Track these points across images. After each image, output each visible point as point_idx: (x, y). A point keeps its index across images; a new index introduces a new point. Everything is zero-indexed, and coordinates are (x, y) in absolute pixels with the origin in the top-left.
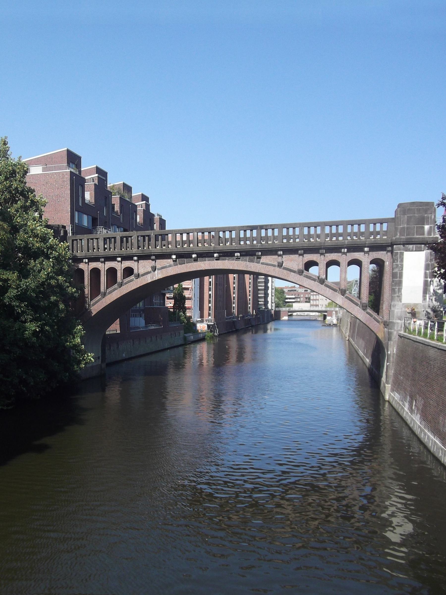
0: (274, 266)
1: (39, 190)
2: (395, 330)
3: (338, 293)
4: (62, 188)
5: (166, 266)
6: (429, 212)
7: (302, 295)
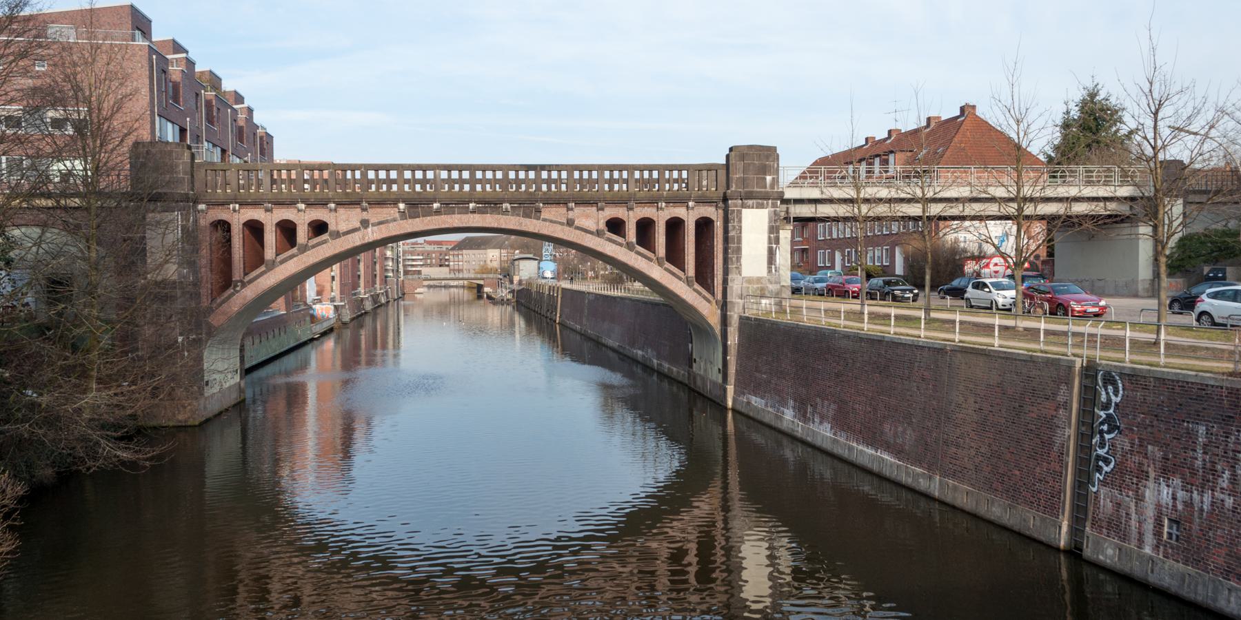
0: (562, 224)
2: (735, 313)
6: (771, 159)
7: (434, 255)
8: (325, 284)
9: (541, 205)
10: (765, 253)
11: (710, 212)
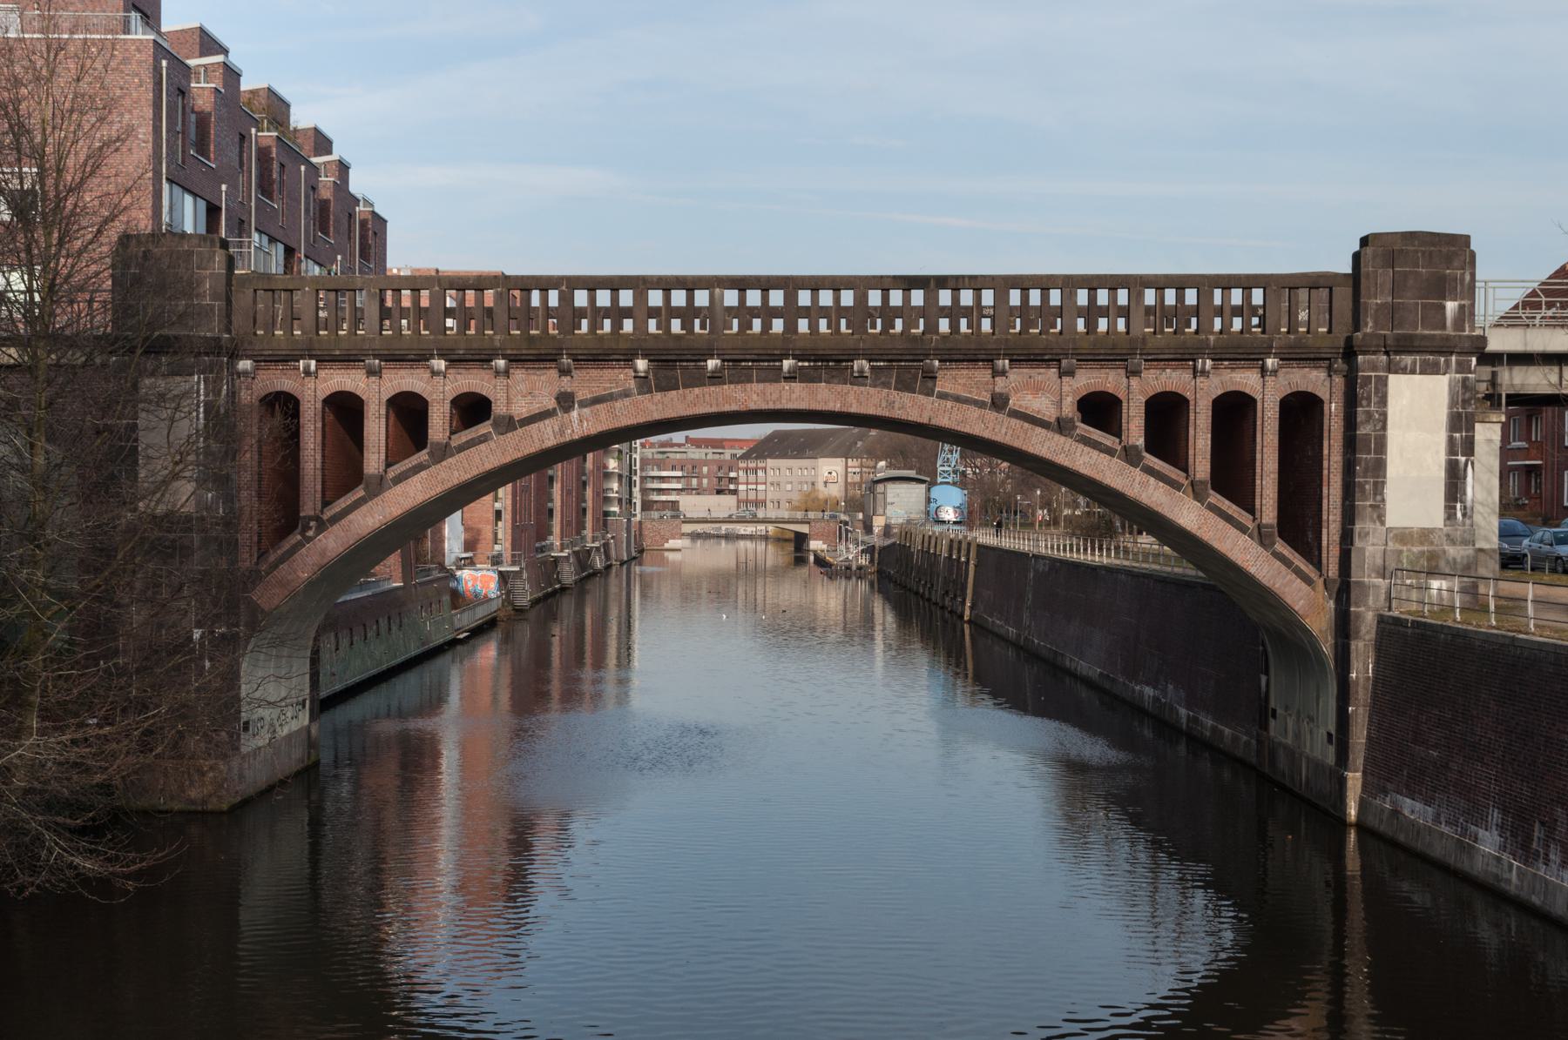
0: (981, 405)
6: (1456, 264)
10: (1440, 474)
11: (1313, 380)
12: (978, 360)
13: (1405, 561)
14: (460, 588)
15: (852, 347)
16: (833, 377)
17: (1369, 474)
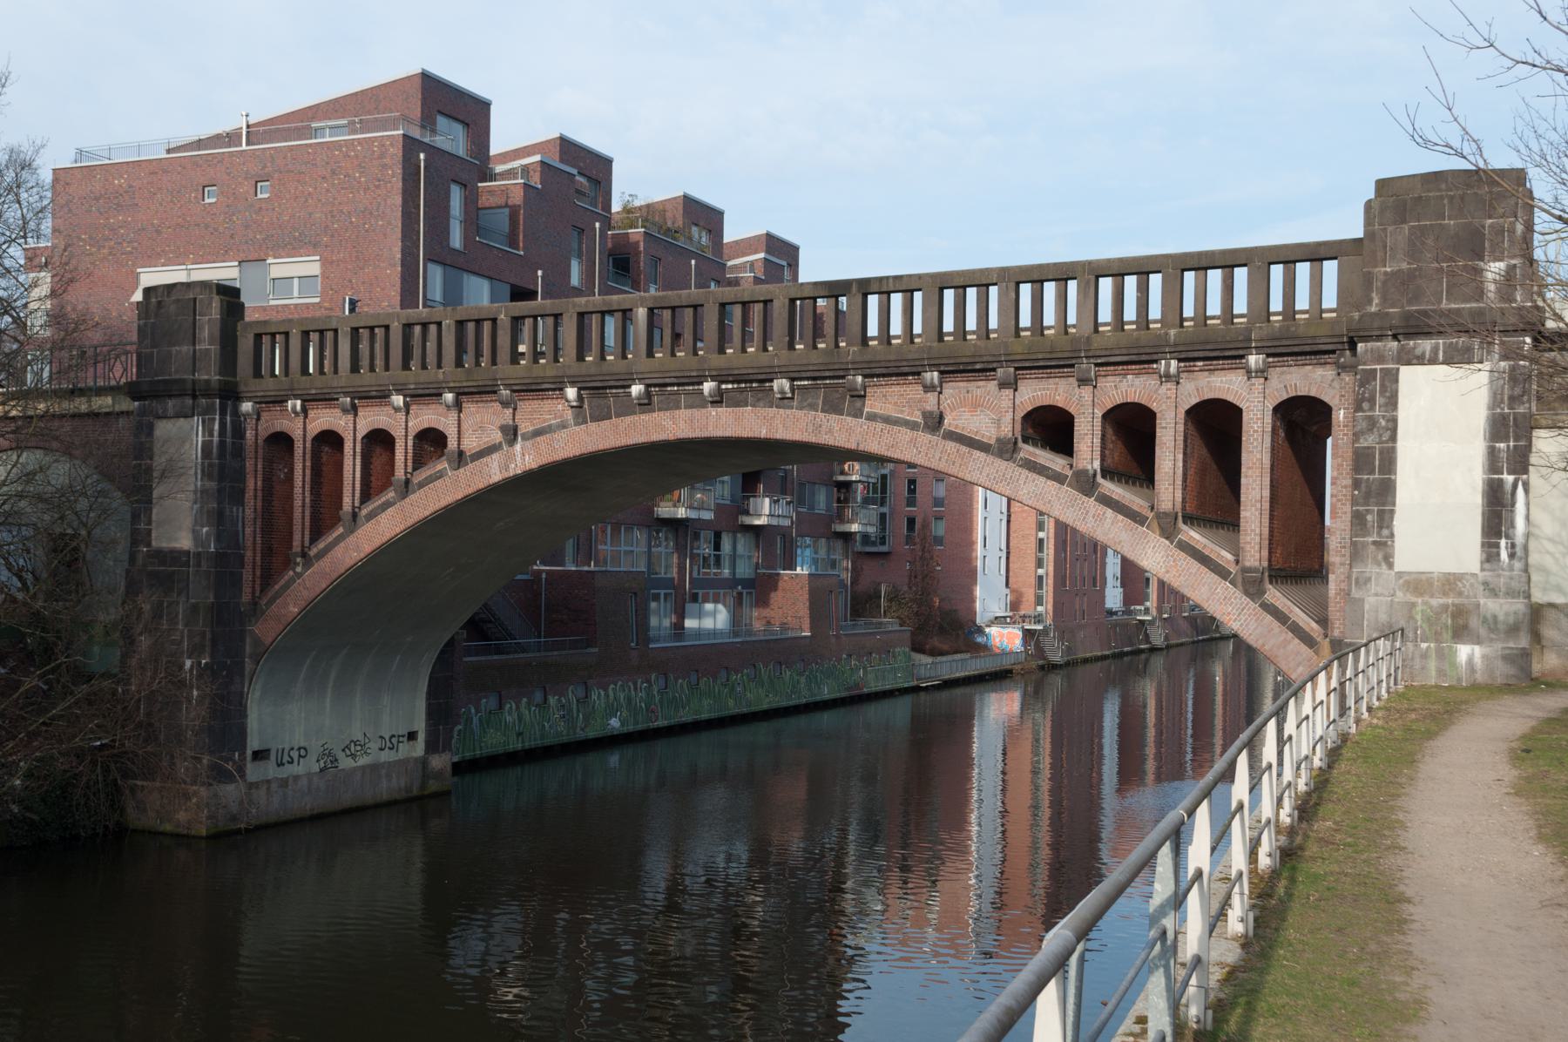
0: (913, 426)
1: (310, 194)
3: (1147, 528)
4: (378, 187)
5: (550, 426)
8: (1024, 590)
9: (859, 379)
10: (1474, 500)
12: (906, 374)
13: (1419, 617)
14: (989, 644)
15: (766, 364)
16: (759, 400)
17: (1372, 500)
